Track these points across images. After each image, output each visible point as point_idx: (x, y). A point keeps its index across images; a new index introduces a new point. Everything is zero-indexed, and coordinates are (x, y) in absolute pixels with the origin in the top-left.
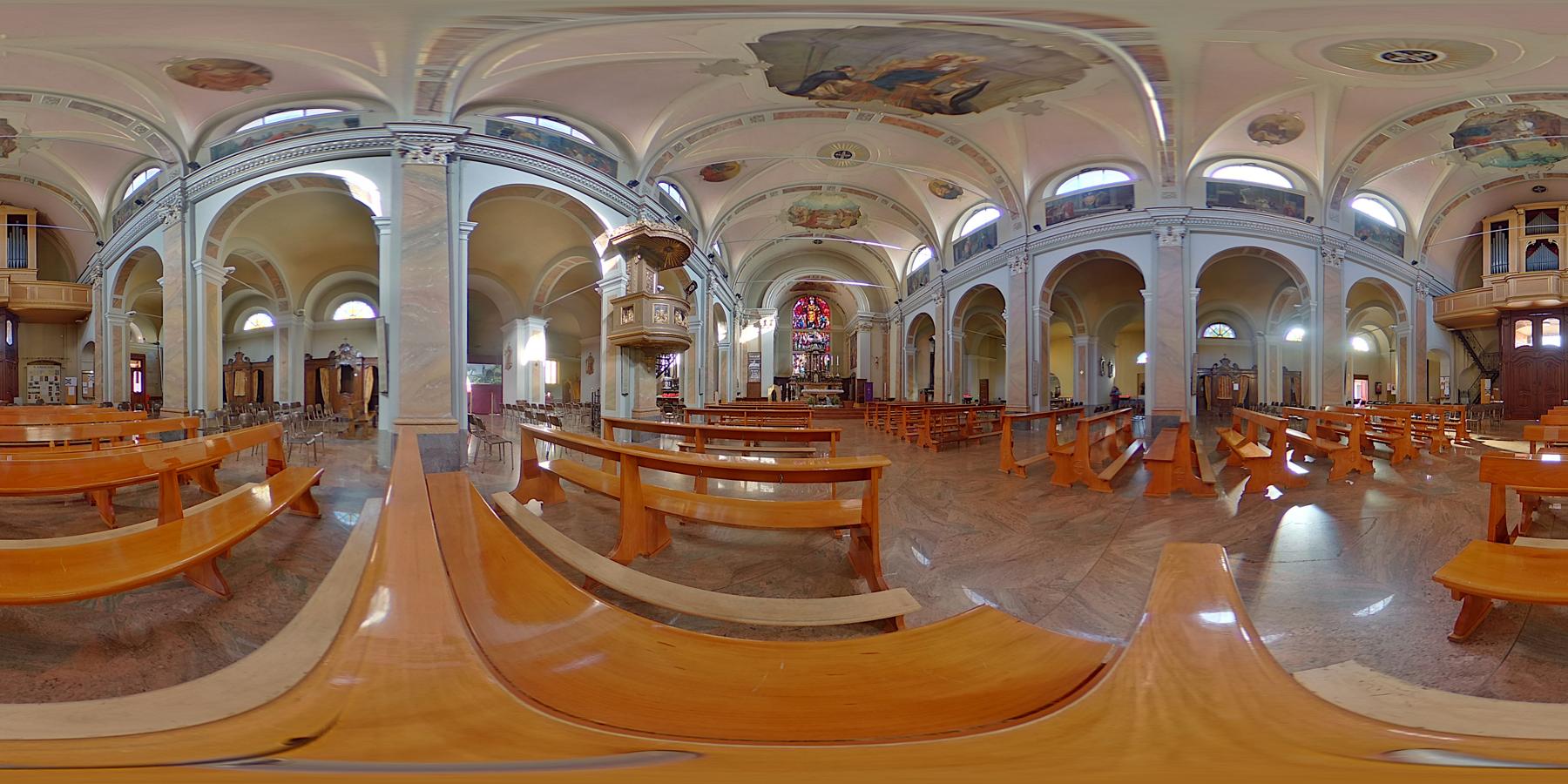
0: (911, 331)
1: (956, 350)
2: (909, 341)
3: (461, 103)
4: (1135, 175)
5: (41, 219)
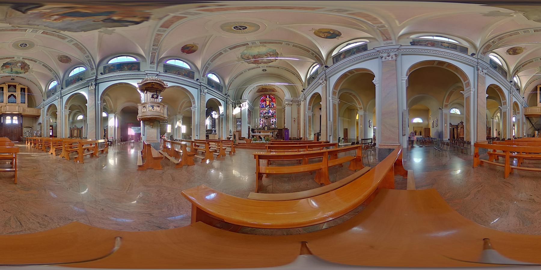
0: (310, 104)
1: (334, 109)
2: (309, 109)
5: (28, 89)
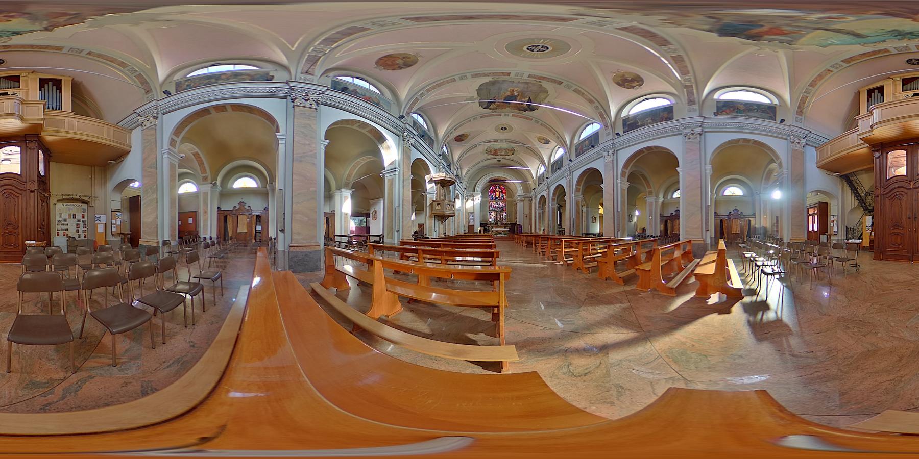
4: (673, 100)
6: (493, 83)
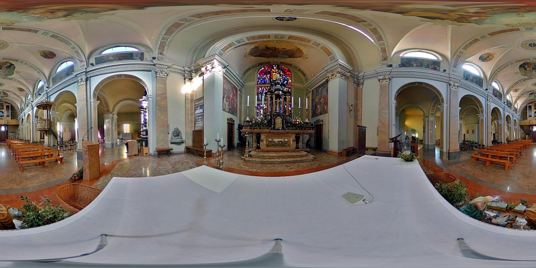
3: (87, 54)
5: (12, 106)
6: (7, 75)
